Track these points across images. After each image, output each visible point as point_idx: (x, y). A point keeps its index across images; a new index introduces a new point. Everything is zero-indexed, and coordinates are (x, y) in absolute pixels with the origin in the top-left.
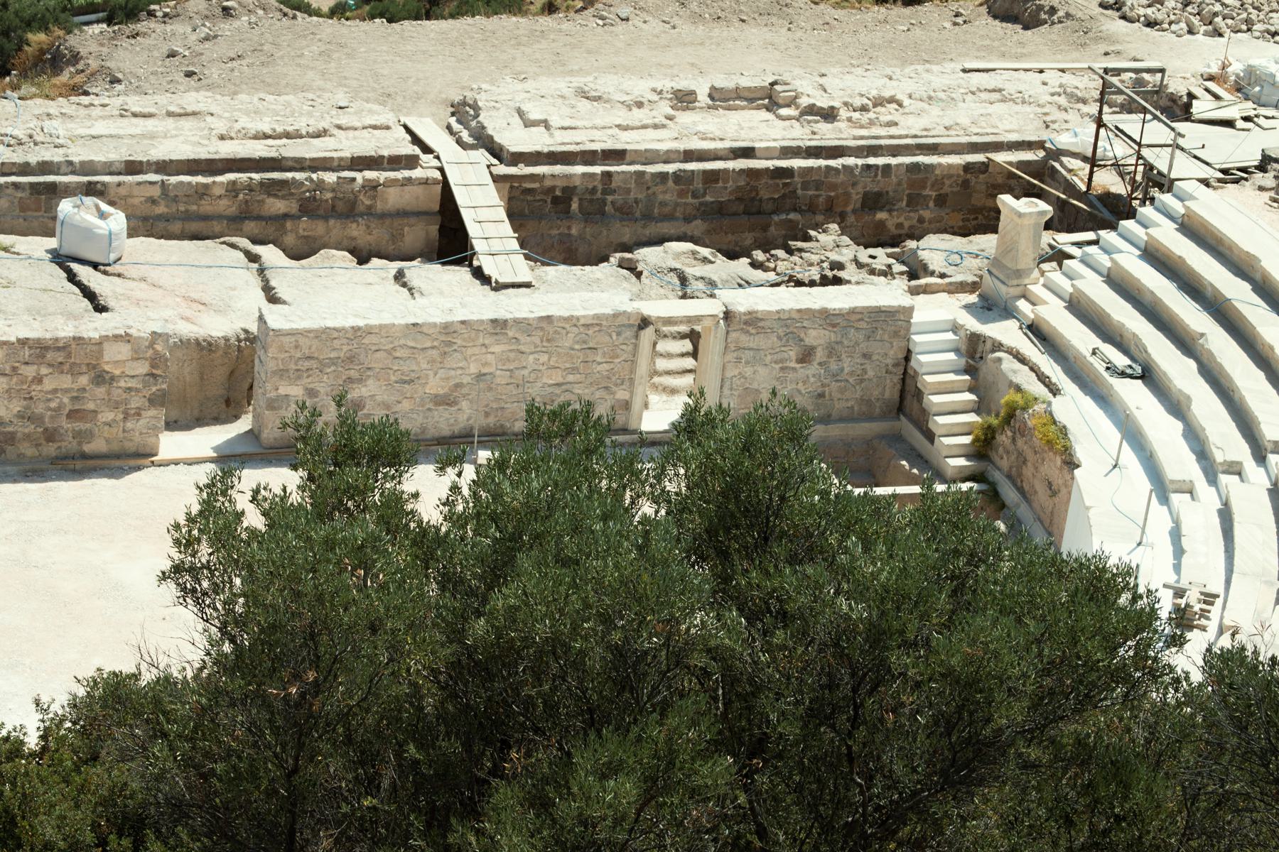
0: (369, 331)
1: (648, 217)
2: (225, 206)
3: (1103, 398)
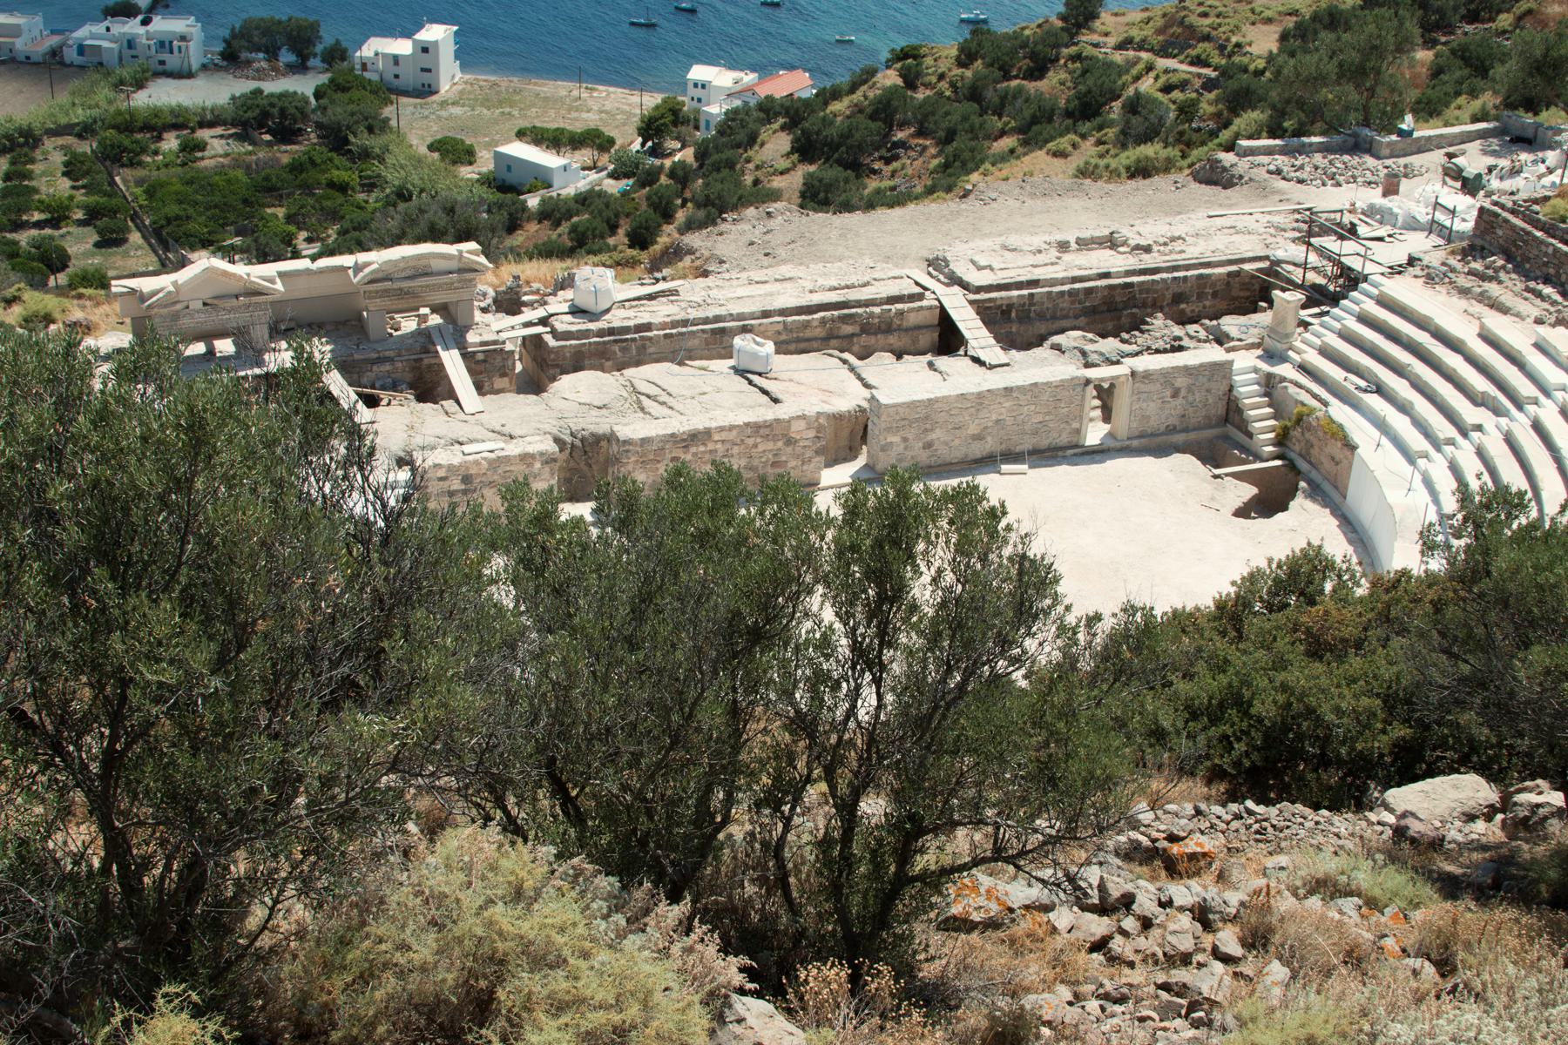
0: (937, 400)
1: (1054, 318)
2: (819, 332)
3: (1356, 406)
